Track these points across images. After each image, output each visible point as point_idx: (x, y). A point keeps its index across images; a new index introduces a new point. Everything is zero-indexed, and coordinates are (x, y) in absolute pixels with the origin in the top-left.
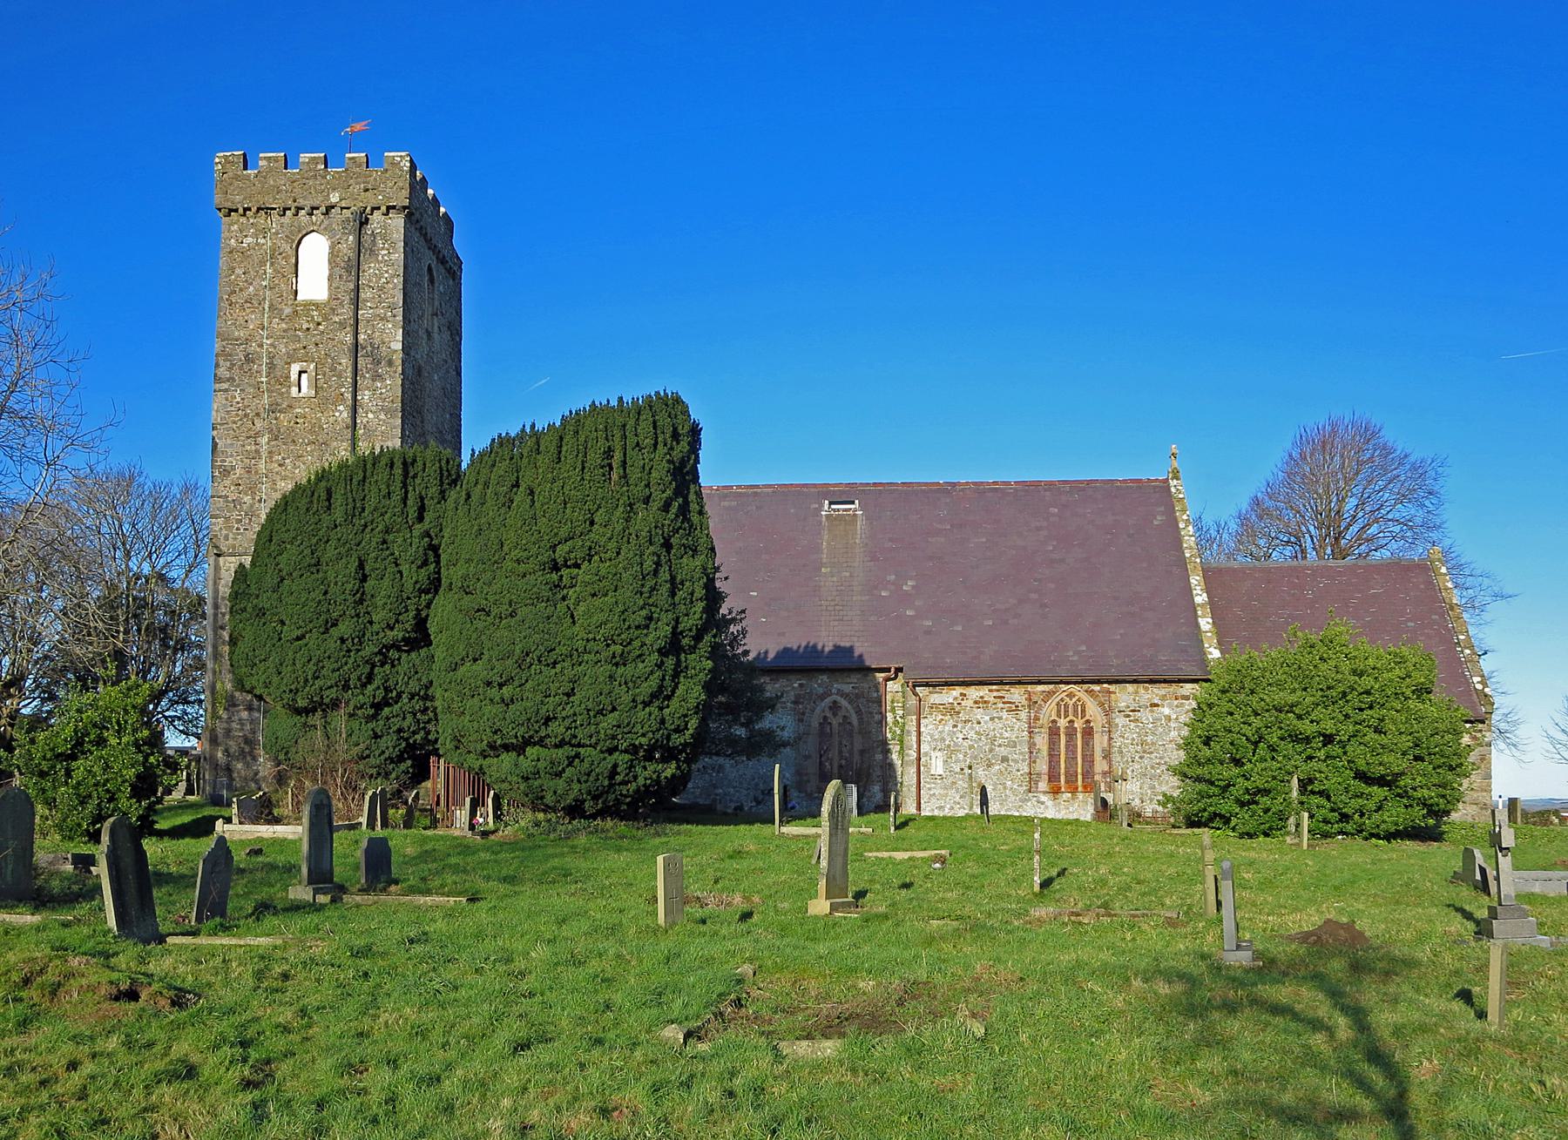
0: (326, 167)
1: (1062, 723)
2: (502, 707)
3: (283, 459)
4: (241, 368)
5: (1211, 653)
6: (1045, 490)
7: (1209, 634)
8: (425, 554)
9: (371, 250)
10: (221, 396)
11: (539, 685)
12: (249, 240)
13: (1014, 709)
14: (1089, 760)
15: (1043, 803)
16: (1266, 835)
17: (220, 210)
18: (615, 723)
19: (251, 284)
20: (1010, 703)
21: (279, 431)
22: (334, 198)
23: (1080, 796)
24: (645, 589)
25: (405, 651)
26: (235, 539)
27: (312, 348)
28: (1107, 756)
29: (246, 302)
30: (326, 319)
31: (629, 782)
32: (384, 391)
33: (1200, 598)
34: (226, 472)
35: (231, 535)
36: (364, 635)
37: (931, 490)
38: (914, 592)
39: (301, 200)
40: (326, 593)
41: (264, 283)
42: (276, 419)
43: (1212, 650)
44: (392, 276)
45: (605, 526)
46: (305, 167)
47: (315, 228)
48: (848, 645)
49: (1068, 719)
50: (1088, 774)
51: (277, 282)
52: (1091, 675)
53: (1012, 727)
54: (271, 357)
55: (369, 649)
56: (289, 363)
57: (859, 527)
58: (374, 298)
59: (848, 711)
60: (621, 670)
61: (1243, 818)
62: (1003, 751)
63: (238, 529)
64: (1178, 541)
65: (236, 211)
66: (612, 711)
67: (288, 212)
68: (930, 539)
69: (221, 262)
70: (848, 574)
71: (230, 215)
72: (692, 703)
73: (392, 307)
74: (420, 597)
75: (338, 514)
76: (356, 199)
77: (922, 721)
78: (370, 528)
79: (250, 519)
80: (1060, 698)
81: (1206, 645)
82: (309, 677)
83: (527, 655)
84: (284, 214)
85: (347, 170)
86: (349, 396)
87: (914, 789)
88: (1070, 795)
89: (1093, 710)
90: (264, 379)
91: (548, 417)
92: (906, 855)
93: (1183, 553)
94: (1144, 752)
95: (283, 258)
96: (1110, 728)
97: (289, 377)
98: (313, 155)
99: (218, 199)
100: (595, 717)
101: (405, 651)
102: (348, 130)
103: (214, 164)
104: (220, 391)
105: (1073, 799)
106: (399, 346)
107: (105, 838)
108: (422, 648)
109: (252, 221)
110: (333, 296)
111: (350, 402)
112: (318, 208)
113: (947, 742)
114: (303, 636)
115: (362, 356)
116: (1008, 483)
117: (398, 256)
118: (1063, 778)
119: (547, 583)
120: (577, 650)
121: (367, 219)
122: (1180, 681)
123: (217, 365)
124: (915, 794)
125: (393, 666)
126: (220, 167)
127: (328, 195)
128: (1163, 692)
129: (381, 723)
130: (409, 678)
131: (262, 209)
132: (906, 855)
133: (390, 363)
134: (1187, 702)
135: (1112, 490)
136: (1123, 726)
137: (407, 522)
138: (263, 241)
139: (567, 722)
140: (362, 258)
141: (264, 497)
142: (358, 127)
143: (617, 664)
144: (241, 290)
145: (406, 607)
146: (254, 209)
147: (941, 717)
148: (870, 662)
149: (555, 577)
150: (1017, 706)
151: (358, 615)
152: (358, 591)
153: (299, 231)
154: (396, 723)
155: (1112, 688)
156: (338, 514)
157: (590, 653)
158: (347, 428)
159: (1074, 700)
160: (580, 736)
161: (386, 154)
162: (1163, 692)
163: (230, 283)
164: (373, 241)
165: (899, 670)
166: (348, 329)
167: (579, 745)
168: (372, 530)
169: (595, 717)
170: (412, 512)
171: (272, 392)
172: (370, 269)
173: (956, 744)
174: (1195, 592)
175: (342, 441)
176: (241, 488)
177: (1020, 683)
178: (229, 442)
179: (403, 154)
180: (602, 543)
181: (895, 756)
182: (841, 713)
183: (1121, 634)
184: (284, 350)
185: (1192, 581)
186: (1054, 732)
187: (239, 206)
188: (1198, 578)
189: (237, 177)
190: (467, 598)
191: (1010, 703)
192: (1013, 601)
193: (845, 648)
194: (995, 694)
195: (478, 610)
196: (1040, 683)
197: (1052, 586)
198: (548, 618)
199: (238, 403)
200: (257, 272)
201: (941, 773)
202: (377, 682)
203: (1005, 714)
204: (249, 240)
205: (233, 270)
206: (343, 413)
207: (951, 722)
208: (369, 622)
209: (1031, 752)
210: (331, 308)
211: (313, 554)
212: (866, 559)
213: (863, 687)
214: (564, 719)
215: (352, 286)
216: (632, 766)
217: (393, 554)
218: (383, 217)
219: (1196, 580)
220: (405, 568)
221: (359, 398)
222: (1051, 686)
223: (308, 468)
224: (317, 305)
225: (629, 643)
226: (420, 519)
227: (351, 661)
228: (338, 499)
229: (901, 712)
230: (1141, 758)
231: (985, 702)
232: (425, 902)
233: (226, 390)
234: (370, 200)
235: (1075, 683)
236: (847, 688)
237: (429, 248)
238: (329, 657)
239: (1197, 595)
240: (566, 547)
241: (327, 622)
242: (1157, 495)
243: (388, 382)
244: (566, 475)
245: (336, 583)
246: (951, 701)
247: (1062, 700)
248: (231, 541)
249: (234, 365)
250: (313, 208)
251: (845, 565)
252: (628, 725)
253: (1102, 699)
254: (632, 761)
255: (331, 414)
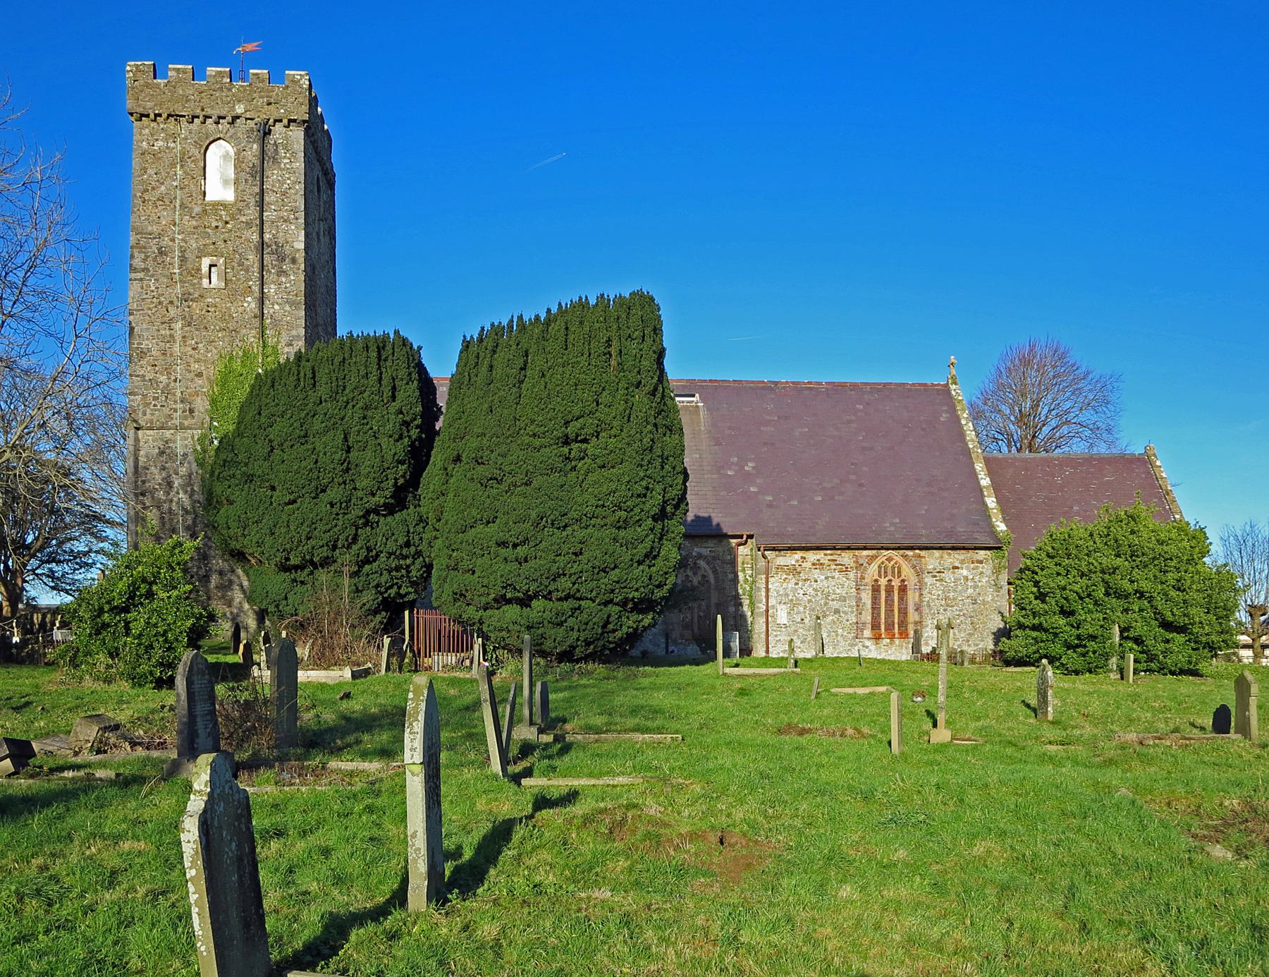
0: (231, 81)
1: (883, 582)
2: (515, 565)
3: (197, 343)
4: (155, 259)
5: (998, 526)
6: (851, 390)
7: (995, 511)
8: (401, 429)
9: (274, 158)
10: (136, 285)
11: (552, 545)
12: (160, 143)
13: (845, 570)
14: (904, 612)
15: (867, 647)
16: (1090, 672)
17: (131, 114)
18: (616, 579)
19: (163, 183)
20: (842, 565)
21: (192, 319)
22: (240, 109)
23: (897, 641)
24: (645, 463)
25: (383, 515)
26: (153, 415)
27: (220, 244)
28: (918, 609)
29: (158, 200)
30: (233, 218)
31: (617, 630)
32: (288, 285)
33: (985, 481)
34: (143, 354)
35: (148, 411)
36: (350, 501)
37: (758, 387)
38: (754, 472)
39: (209, 110)
40: (316, 462)
41: (175, 184)
42: (189, 307)
43: (998, 523)
44: (294, 183)
45: (609, 406)
46: (213, 80)
47: (222, 136)
48: (706, 515)
49: (887, 579)
50: (903, 624)
51: (186, 183)
52: (907, 542)
53: (842, 585)
54: (183, 251)
55: (356, 512)
56: (200, 257)
57: (702, 417)
58: (277, 201)
59: (705, 571)
60: (622, 533)
61: (1071, 658)
62: (835, 605)
63: (155, 405)
64: (962, 435)
65: (148, 116)
66: (613, 569)
67: (196, 120)
68: (762, 428)
69: (134, 162)
70: (698, 456)
71: (141, 120)
72: (673, 562)
73: (294, 211)
74: (398, 467)
75: (323, 390)
76: (260, 111)
77: (770, 579)
78: (351, 404)
79: (167, 397)
80: (881, 561)
81: (994, 520)
82: (303, 537)
83: (542, 519)
84: (192, 122)
85: (251, 84)
86: (256, 289)
87: (763, 636)
88: (888, 640)
89: (907, 571)
90: (177, 271)
91: (534, 310)
92: (867, 690)
93: (967, 444)
94: (947, 606)
95: (192, 161)
96: (921, 587)
97: (199, 270)
98: (219, 69)
99: (130, 104)
100: (598, 573)
101: (383, 515)
102: (240, 49)
103: (125, 72)
104: (135, 280)
105: (891, 644)
106: (302, 246)
107: (180, 682)
108: (396, 512)
109: (162, 126)
110: (240, 199)
111: (257, 294)
112: (224, 118)
113: (790, 597)
114: (294, 502)
115: (268, 253)
116: (820, 383)
117: (299, 165)
118: (883, 627)
119: (560, 456)
120: (585, 515)
121: (270, 130)
122: (975, 548)
123: (132, 257)
124: (764, 640)
125: (372, 528)
126: (131, 74)
127: (234, 106)
128: (962, 557)
129: (362, 578)
130: (387, 539)
131: (172, 116)
132: (867, 690)
133: (294, 261)
134: (981, 565)
135: (903, 390)
136: (931, 585)
137: (383, 401)
138: (172, 145)
139: (574, 578)
140: (265, 165)
141: (179, 377)
142: (250, 47)
143: (619, 528)
144: (153, 189)
145: (386, 476)
146: (165, 116)
147: (785, 576)
148: (727, 530)
149: (566, 450)
150: (847, 568)
151: (344, 483)
152: (345, 461)
153: (207, 138)
154: (375, 579)
155: (923, 553)
156: (323, 390)
157: (597, 518)
158: (255, 317)
159: (892, 563)
160: (583, 590)
161: (287, 72)
162: (962, 557)
163: (143, 182)
164: (276, 150)
165: (751, 537)
166: (254, 228)
167: (580, 599)
168: (354, 406)
169: (598, 573)
170: (387, 393)
171: (185, 282)
172: (273, 175)
173: (797, 599)
174: (980, 476)
175: (251, 329)
176: (157, 368)
177: (849, 548)
178: (145, 326)
179: (303, 73)
180: (608, 422)
181: (746, 608)
182: (702, 572)
183: (925, 510)
184: (194, 245)
185: (977, 467)
186: (876, 589)
187: (150, 111)
188: (981, 465)
189: (147, 85)
190: (480, 468)
191: (842, 565)
192: (836, 481)
193: (703, 517)
194: (829, 557)
195: (491, 479)
196: (865, 548)
197: (865, 469)
198: (562, 486)
199: (153, 291)
200: (168, 173)
201: (786, 622)
202: (360, 543)
203: (837, 574)
204: (160, 143)
205: (145, 170)
206: (251, 304)
207: (794, 581)
208: (353, 488)
209: (858, 606)
210: (238, 209)
211: (302, 426)
212: (711, 444)
213: (718, 551)
214: (571, 575)
215: (257, 190)
216: (620, 617)
217: (372, 429)
218: (285, 129)
219: (979, 467)
220: (384, 441)
221: (266, 291)
222: (874, 552)
223: (220, 352)
224: (223, 205)
225: (632, 510)
226: (394, 398)
227: (340, 523)
228: (322, 377)
229: (750, 572)
230: (945, 610)
231: (821, 564)
232: (644, 739)
233: (141, 280)
234: (273, 112)
235: (893, 549)
236: (705, 552)
237: (318, 160)
238: (321, 520)
239: (982, 479)
240: (577, 424)
241: (317, 488)
242: (941, 397)
243: (292, 278)
244: (574, 360)
245: (325, 454)
246: (793, 563)
247: (882, 563)
248: (148, 416)
249: (148, 257)
250: (220, 118)
251: (694, 448)
252: (625, 581)
253: (915, 562)
254: (620, 611)
255: (240, 304)
